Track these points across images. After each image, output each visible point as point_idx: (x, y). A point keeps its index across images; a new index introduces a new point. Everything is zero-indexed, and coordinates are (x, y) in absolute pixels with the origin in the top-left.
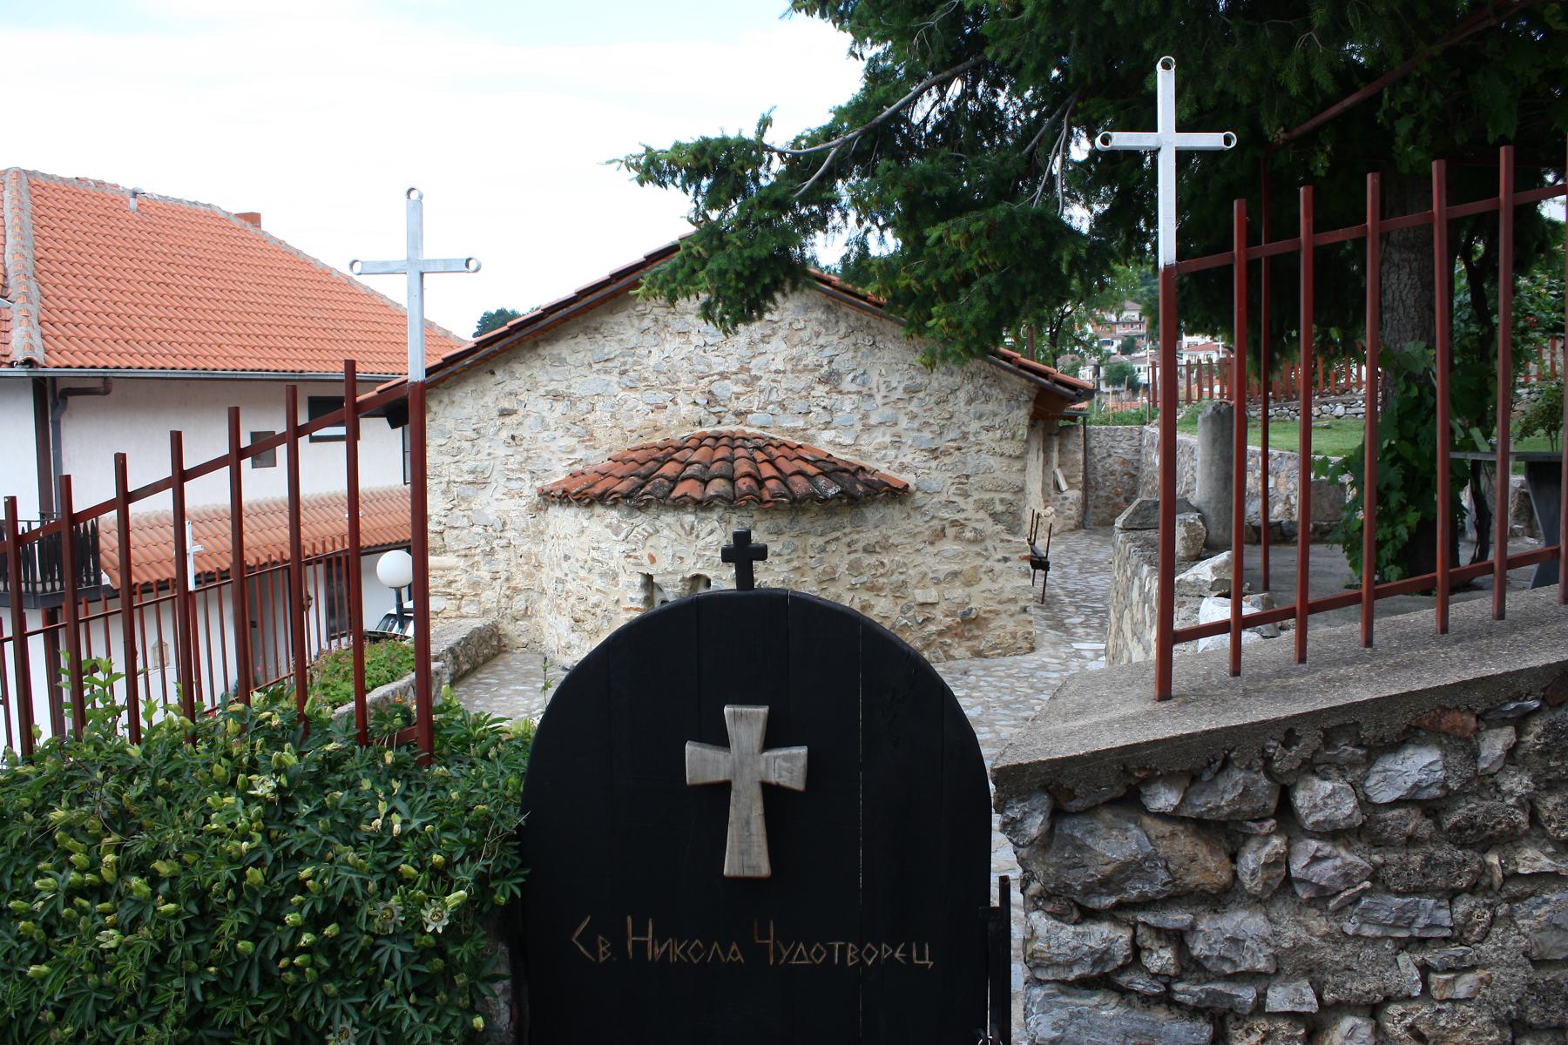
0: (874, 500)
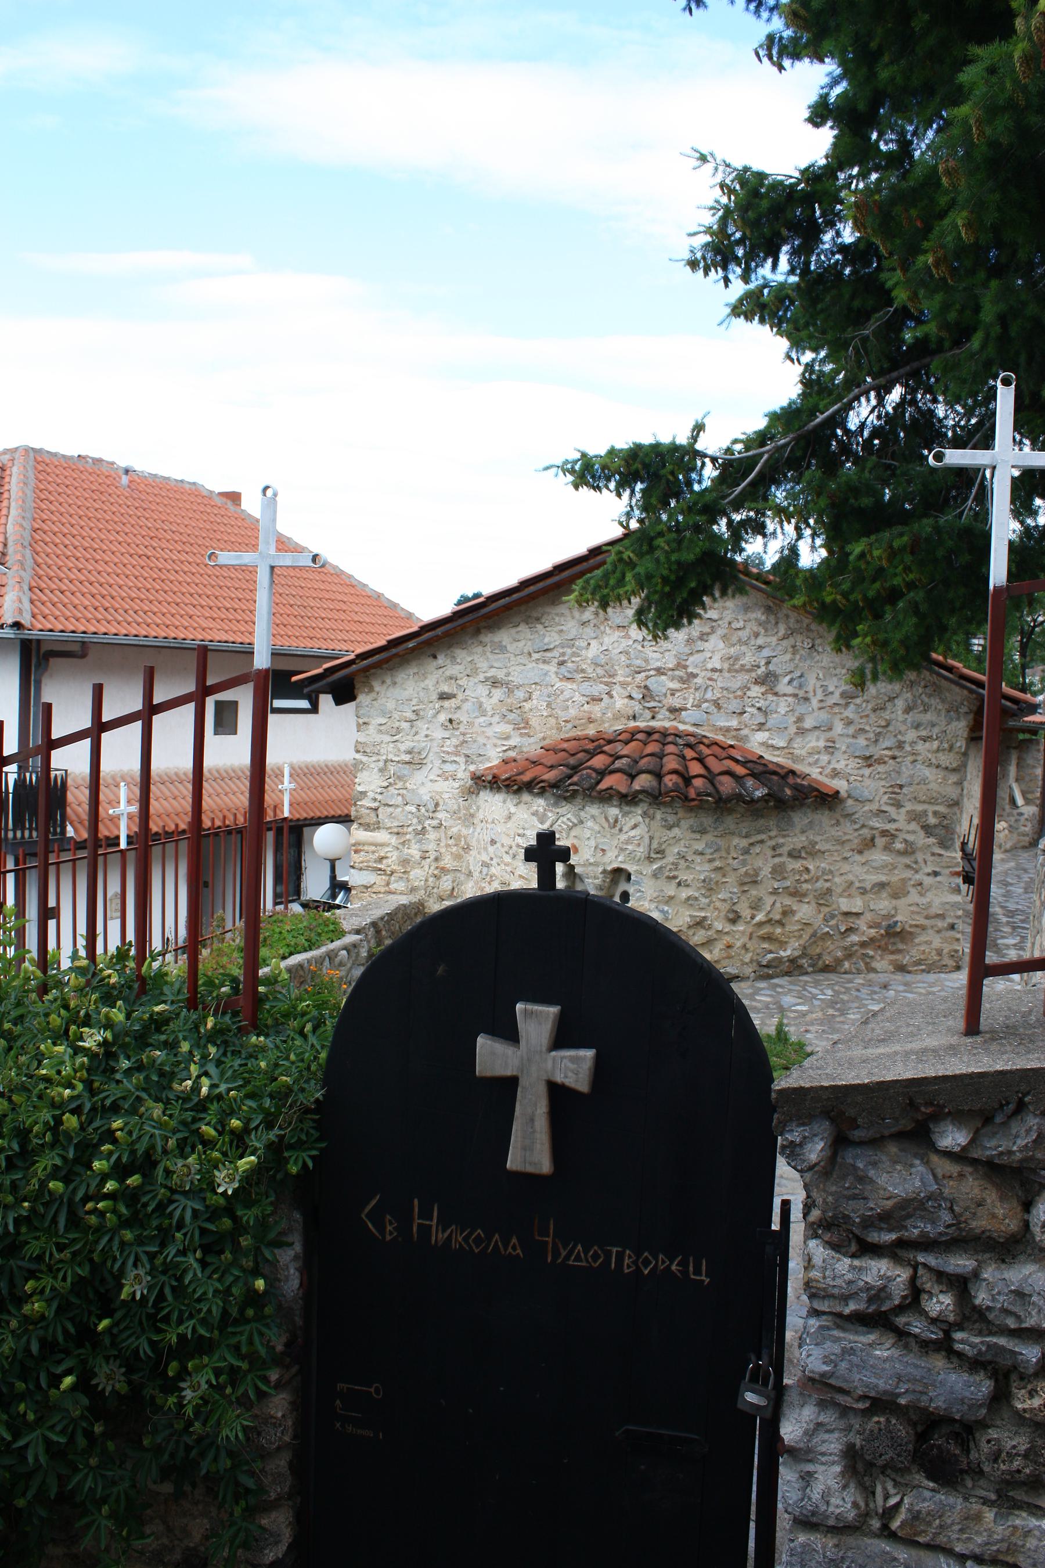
0: (802, 805)
